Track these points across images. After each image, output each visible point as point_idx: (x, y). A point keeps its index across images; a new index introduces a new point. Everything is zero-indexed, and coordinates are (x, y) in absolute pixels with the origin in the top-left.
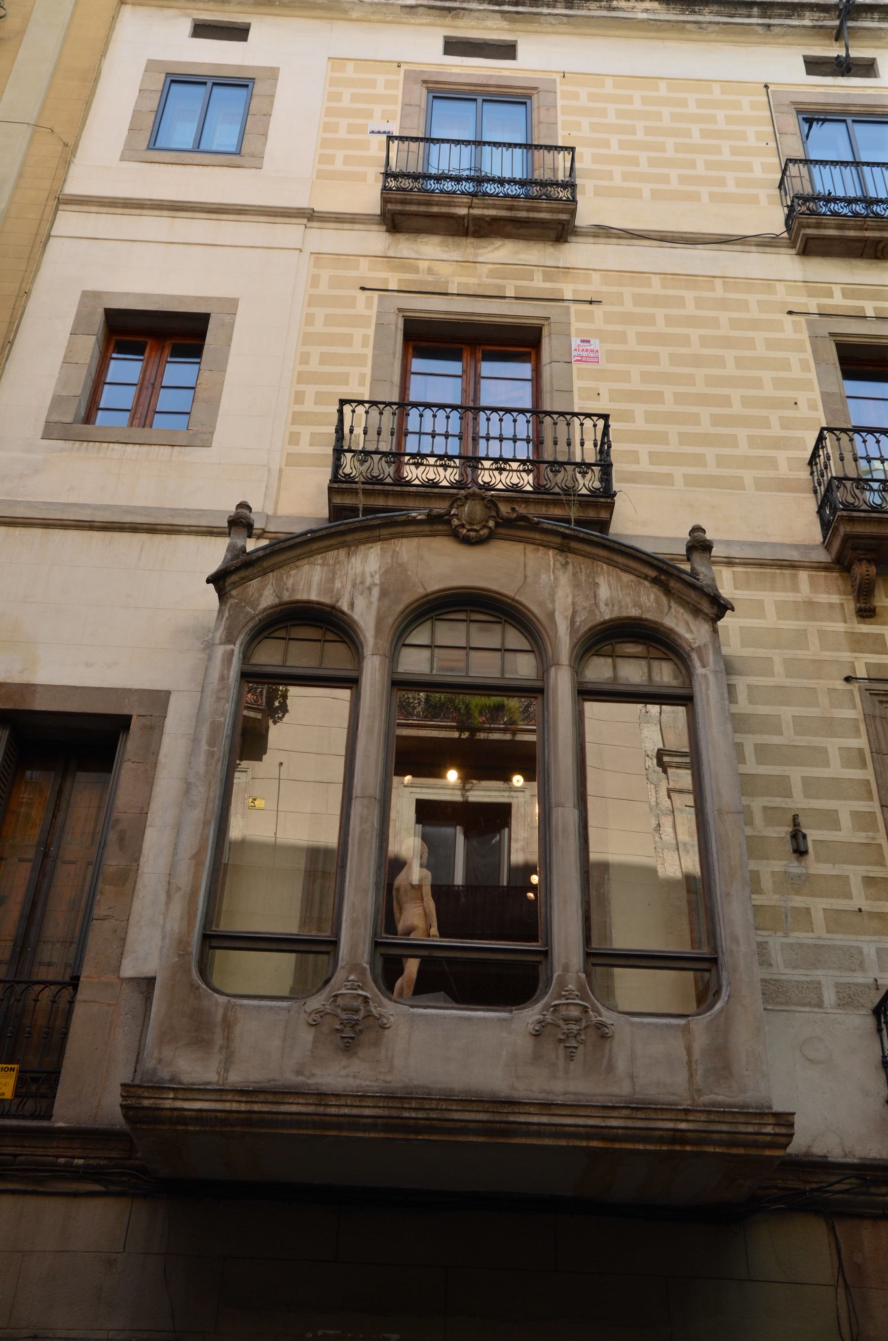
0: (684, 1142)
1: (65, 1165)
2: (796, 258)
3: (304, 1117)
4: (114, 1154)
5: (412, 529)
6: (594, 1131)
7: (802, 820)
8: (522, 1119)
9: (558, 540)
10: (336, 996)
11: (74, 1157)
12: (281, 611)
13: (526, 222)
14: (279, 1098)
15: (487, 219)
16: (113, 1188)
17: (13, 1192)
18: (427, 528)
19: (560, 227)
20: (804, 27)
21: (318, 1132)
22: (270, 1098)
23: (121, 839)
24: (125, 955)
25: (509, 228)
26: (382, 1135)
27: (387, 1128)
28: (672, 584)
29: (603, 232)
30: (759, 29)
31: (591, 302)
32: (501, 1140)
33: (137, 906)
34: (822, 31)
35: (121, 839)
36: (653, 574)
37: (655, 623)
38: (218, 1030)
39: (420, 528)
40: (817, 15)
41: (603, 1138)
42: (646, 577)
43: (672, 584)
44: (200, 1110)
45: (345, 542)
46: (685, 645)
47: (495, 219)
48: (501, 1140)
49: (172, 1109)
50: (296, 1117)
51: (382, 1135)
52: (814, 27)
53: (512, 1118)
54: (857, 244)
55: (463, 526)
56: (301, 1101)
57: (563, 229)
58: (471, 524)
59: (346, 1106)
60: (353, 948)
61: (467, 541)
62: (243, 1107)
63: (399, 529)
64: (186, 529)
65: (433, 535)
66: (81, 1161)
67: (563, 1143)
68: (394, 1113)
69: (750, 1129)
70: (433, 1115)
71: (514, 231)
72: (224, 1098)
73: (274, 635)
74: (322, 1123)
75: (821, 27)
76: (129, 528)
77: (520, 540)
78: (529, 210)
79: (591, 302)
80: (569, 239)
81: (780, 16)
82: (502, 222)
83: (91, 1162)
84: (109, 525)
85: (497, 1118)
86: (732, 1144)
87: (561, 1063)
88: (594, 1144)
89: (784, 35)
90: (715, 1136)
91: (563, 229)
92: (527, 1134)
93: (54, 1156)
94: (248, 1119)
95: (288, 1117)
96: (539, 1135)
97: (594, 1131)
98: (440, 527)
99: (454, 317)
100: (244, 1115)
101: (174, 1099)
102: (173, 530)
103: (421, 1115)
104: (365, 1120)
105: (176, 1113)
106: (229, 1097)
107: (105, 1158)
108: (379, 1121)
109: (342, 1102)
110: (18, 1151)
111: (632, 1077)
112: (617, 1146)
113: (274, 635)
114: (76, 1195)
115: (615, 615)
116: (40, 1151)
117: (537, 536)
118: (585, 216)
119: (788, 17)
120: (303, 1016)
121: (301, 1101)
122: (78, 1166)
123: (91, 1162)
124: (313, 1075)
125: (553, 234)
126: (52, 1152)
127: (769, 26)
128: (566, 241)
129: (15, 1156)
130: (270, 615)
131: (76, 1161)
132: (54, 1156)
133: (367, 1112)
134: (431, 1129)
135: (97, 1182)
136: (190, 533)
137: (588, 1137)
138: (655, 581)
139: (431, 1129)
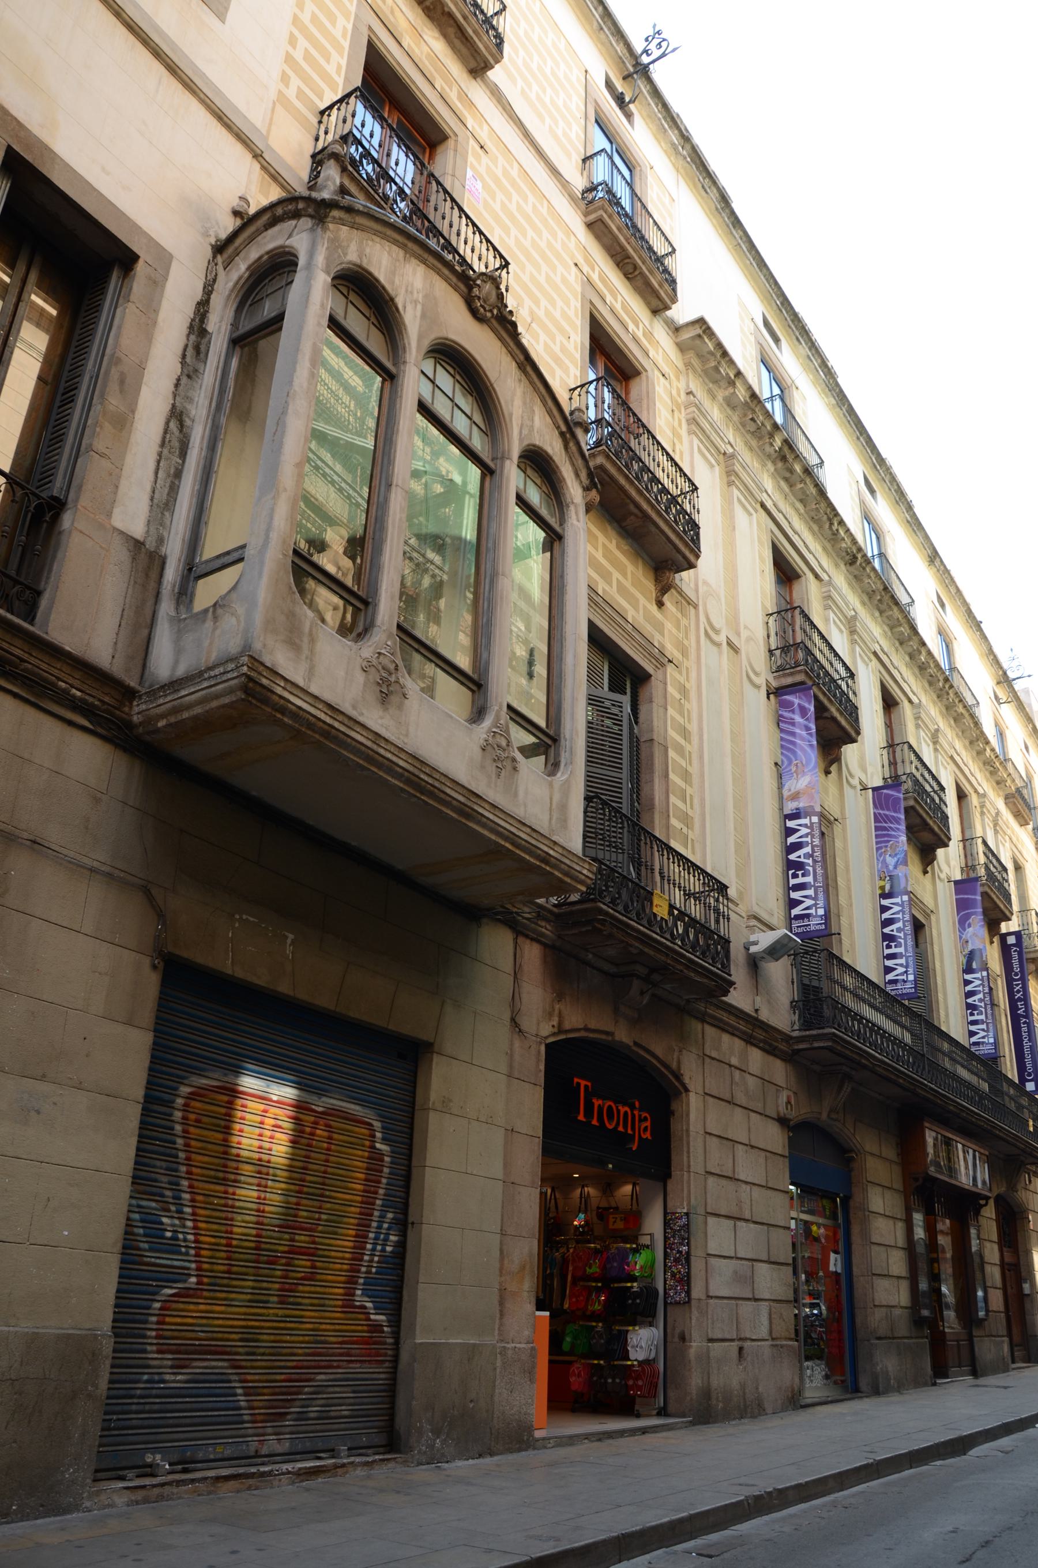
0: (547, 863)
1: (64, 690)
2: (584, 226)
3: (363, 748)
4: (107, 699)
5: (446, 272)
6: (511, 836)
7: (536, 653)
8: (481, 810)
9: (522, 357)
10: (379, 653)
11: (72, 686)
12: (357, 272)
13: (466, 39)
14: (351, 724)
15: (446, 9)
16: (99, 730)
17: (15, 695)
18: (454, 280)
19: (483, 65)
20: (616, 51)
21: (365, 764)
22: (346, 721)
23: (122, 382)
24: (116, 504)
25: (451, 31)
26: (401, 785)
27: (408, 782)
28: (571, 444)
29: (496, 94)
30: (595, 23)
31: (482, 147)
32: (464, 821)
33: (129, 459)
34: (621, 65)
35: (122, 382)
36: (564, 429)
37: (557, 467)
38: (306, 640)
39: (451, 276)
40: (625, 51)
41: (513, 844)
42: (558, 428)
43: (571, 444)
44: (300, 708)
45: (406, 246)
46: (568, 496)
47: (450, 15)
48: (464, 821)
49: (281, 697)
50: (358, 745)
51: (401, 785)
52: (621, 58)
53: (476, 807)
54: (618, 248)
55: (479, 298)
56: (364, 733)
57: (483, 68)
58: (485, 301)
59: (390, 752)
60: (384, 616)
61: (474, 312)
62: (328, 720)
63: (439, 266)
64: (202, 95)
65: (456, 289)
66: (78, 694)
67: (493, 837)
68: (416, 772)
69: (578, 868)
70: (437, 784)
71: (453, 36)
72: (317, 705)
73: (339, 287)
74: (372, 758)
75: (623, 62)
76: (153, 49)
77: (501, 339)
78: (475, 31)
79: (482, 147)
80: (478, 79)
81: (609, 29)
82: (452, 22)
83: (87, 697)
84: (136, 28)
85: (469, 804)
86: (567, 874)
87: (494, 776)
88: (507, 845)
89: (603, 44)
90: (563, 866)
91: (483, 68)
92: (479, 823)
93: (57, 678)
94: (328, 732)
95: (354, 743)
96: (484, 826)
97: (511, 836)
98: (462, 286)
99: (401, 71)
100: (326, 727)
101: (284, 688)
102: (189, 86)
103: (430, 781)
104: (398, 769)
105: (282, 702)
106: (320, 707)
107: (99, 700)
108: (406, 774)
109: (388, 747)
110: (26, 656)
111: (525, 806)
112: (518, 852)
113: (339, 287)
114: (70, 723)
115: (541, 445)
116: (44, 666)
117: (512, 344)
118: (495, 74)
119: (612, 34)
120: (359, 660)
121: (364, 733)
122: (74, 696)
123: (87, 697)
124: (363, 714)
125: (473, 64)
126: (56, 672)
127: (602, 29)
128: (475, 79)
129: (22, 660)
130: (349, 269)
131: (74, 691)
132: (57, 678)
133: (401, 763)
134: (431, 795)
135: (85, 716)
136: (202, 102)
137: (506, 839)
138: (562, 434)
139: (431, 795)
